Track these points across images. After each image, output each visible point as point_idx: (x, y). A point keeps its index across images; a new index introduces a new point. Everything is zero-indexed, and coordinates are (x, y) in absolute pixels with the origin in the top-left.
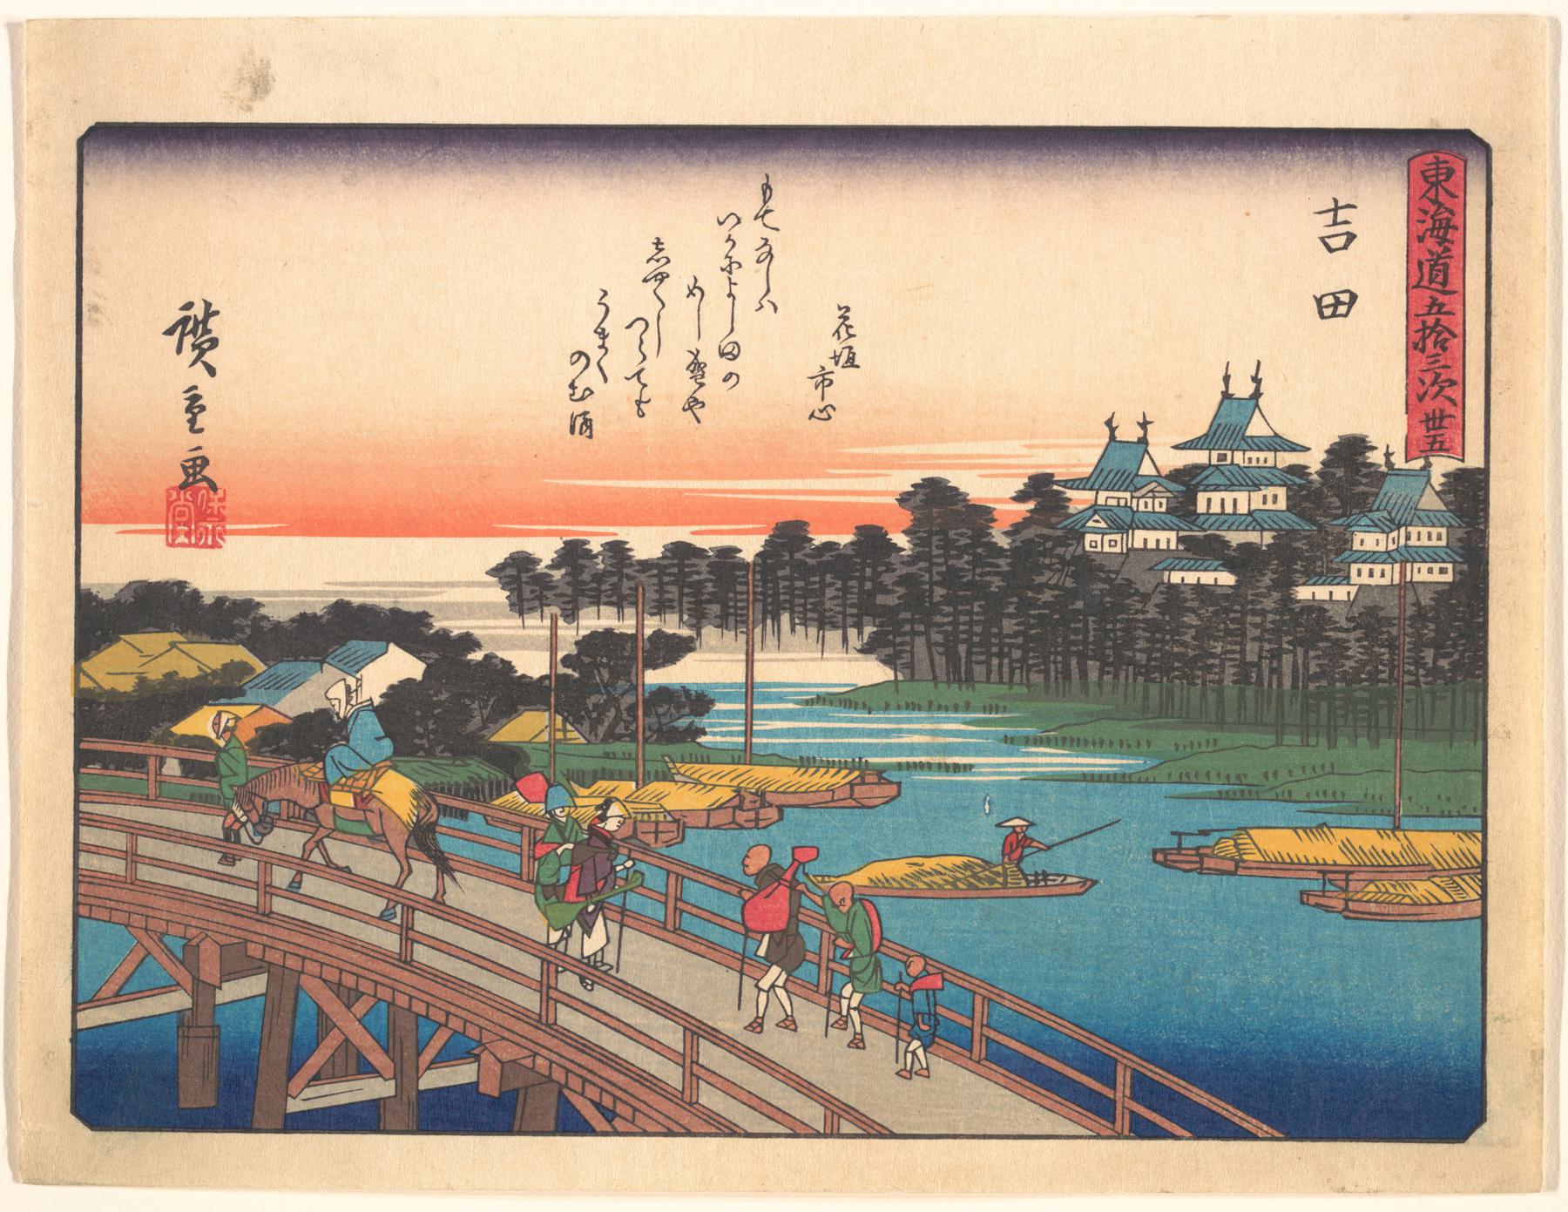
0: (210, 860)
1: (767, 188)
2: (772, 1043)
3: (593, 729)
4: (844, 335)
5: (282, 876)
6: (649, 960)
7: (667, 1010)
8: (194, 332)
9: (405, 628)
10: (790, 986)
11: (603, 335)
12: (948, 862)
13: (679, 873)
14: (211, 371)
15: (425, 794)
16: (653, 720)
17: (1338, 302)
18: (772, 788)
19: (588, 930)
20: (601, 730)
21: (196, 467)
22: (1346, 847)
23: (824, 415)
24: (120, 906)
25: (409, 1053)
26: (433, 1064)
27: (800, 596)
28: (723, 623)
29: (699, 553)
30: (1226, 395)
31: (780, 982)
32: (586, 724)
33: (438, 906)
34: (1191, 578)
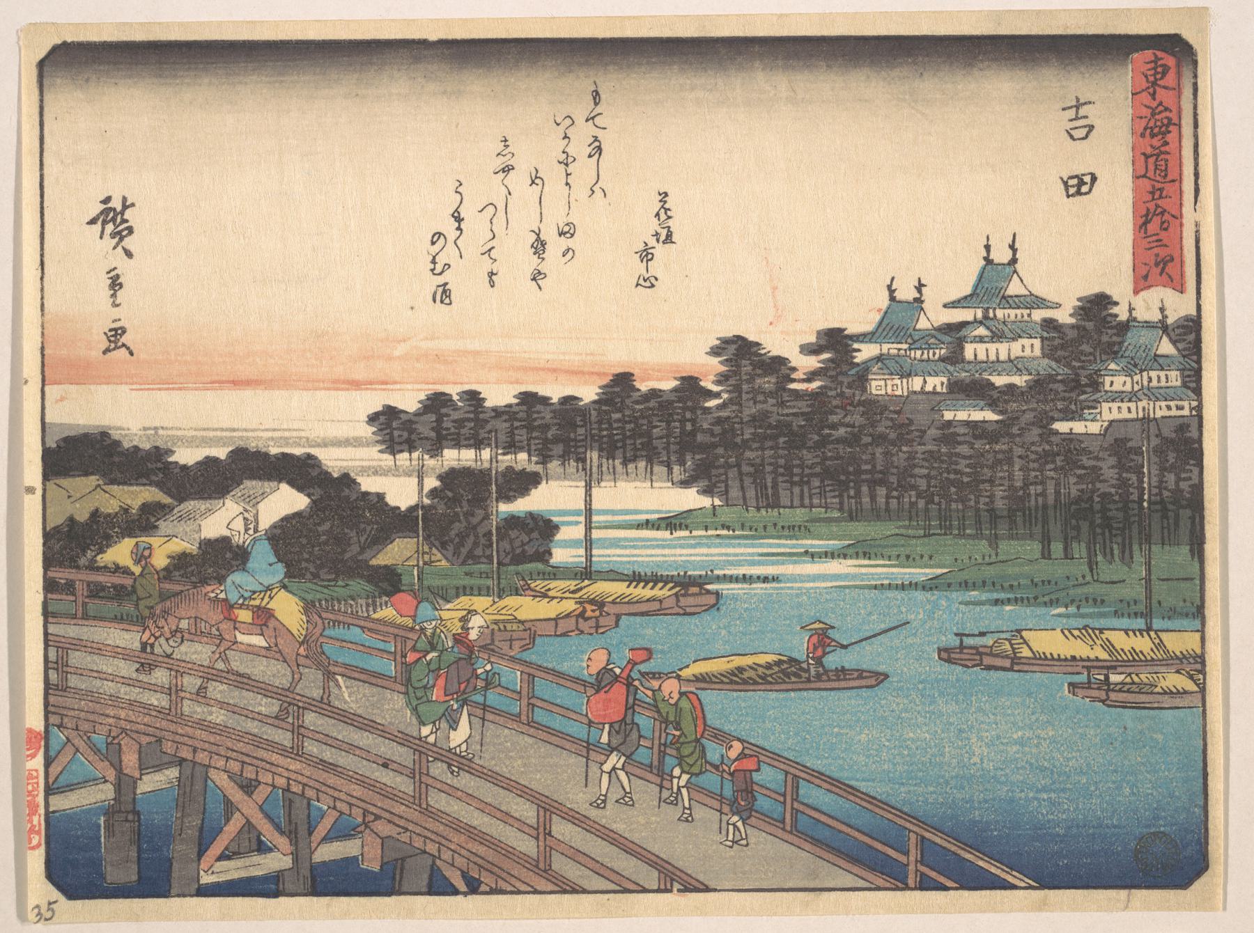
0: (127, 669)
1: (596, 97)
2: (611, 817)
3: (456, 553)
4: (663, 217)
5: (191, 683)
6: (516, 753)
7: (525, 792)
8: (114, 220)
9: (298, 470)
10: (628, 768)
11: (459, 219)
12: (763, 659)
13: (532, 672)
14: (129, 254)
15: (308, 607)
16: (506, 545)
17: (1081, 183)
18: (610, 599)
19: (454, 725)
20: (464, 551)
21: (116, 335)
22: (1109, 646)
23: (648, 284)
24: (396, 820)
25: (303, 831)
26: (326, 839)
27: (630, 437)
28: (564, 458)
29: (545, 400)
30: (988, 261)
31: (619, 765)
32: (451, 548)
33: (324, 706)
34: (962, 416)
